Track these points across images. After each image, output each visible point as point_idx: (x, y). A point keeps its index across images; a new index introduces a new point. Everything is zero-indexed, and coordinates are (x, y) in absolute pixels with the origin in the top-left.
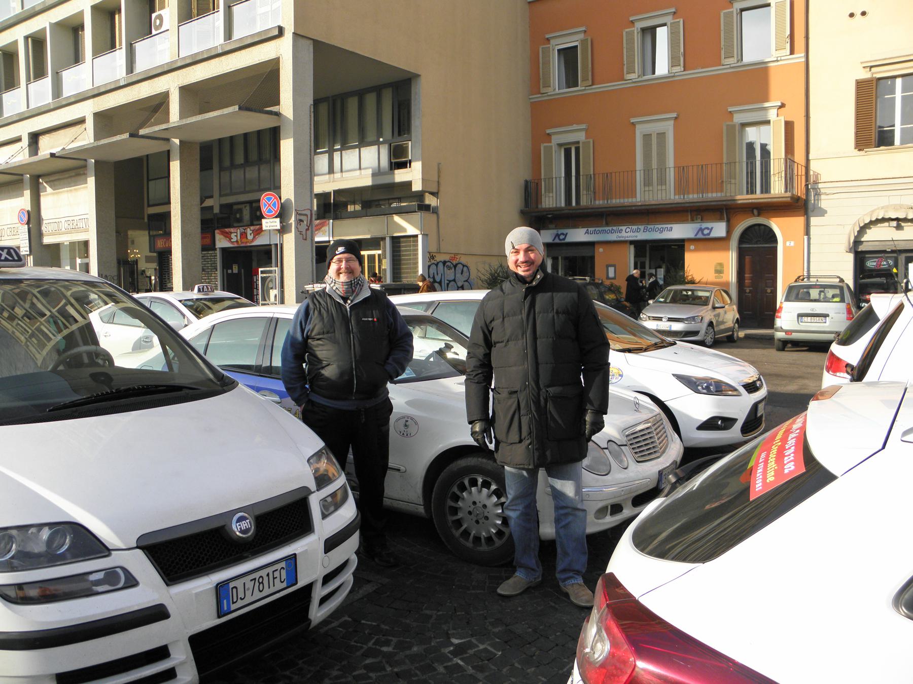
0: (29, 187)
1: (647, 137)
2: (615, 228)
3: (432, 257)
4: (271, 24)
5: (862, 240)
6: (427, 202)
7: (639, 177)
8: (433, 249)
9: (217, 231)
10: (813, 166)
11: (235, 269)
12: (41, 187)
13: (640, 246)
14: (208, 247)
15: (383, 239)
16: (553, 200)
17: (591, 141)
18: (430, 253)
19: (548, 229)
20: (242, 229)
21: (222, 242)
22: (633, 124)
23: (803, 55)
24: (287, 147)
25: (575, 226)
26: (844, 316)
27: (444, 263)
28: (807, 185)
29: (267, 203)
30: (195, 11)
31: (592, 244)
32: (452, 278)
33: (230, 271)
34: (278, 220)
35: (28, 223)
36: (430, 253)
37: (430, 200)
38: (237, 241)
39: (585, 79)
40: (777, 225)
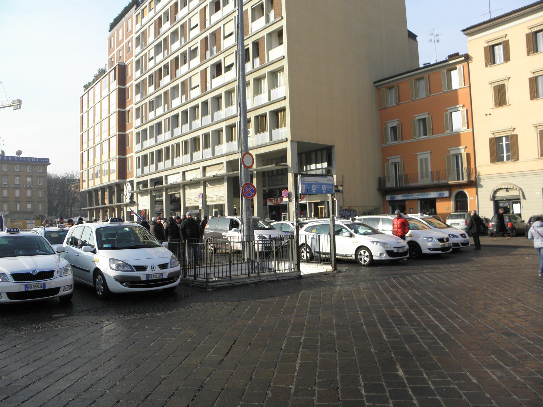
0: (202, 185)
1: (421, 160)
2: (411, 194)
3: (341, 208)
4: (284, 137)
5: (496, 196)
6: (339, 189)
7: (419, 175)
8: (341, 205)
9: (267, 199)
10: (478, 169)
11: (274, 213)
12: (206, 185)
13: (421, 200)
14: (265, 204)
15: (325, 202)
16: (391, 184)
17: (402, 162)
18: (340, 206)
19: (389, 195)
20: (276, 198)
21: (269, 203)
22: (417, 155)
23: (471, 129)
24: (290, 176)
25: (398, 194)
26: (464, 224)
27: (346, 210)
28: (476, 177)
29: (284, 192)
30: (260, 130)
31: (404, 201)
32: (349, 215)
33: (272, 214)
34: (287, 198)
35: (202, 198)
36: (340, 206)
37: (340, 188)
38: (275, 203)
39: (399, 139)
40: (466, 191)
